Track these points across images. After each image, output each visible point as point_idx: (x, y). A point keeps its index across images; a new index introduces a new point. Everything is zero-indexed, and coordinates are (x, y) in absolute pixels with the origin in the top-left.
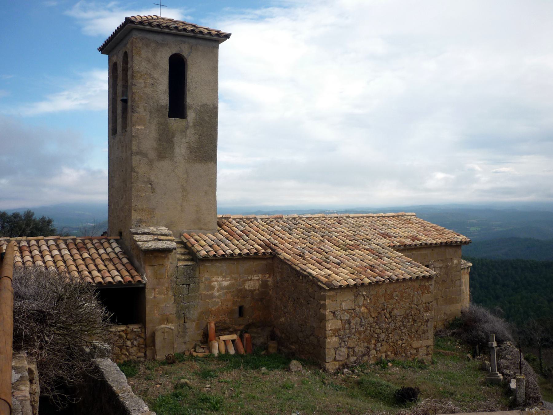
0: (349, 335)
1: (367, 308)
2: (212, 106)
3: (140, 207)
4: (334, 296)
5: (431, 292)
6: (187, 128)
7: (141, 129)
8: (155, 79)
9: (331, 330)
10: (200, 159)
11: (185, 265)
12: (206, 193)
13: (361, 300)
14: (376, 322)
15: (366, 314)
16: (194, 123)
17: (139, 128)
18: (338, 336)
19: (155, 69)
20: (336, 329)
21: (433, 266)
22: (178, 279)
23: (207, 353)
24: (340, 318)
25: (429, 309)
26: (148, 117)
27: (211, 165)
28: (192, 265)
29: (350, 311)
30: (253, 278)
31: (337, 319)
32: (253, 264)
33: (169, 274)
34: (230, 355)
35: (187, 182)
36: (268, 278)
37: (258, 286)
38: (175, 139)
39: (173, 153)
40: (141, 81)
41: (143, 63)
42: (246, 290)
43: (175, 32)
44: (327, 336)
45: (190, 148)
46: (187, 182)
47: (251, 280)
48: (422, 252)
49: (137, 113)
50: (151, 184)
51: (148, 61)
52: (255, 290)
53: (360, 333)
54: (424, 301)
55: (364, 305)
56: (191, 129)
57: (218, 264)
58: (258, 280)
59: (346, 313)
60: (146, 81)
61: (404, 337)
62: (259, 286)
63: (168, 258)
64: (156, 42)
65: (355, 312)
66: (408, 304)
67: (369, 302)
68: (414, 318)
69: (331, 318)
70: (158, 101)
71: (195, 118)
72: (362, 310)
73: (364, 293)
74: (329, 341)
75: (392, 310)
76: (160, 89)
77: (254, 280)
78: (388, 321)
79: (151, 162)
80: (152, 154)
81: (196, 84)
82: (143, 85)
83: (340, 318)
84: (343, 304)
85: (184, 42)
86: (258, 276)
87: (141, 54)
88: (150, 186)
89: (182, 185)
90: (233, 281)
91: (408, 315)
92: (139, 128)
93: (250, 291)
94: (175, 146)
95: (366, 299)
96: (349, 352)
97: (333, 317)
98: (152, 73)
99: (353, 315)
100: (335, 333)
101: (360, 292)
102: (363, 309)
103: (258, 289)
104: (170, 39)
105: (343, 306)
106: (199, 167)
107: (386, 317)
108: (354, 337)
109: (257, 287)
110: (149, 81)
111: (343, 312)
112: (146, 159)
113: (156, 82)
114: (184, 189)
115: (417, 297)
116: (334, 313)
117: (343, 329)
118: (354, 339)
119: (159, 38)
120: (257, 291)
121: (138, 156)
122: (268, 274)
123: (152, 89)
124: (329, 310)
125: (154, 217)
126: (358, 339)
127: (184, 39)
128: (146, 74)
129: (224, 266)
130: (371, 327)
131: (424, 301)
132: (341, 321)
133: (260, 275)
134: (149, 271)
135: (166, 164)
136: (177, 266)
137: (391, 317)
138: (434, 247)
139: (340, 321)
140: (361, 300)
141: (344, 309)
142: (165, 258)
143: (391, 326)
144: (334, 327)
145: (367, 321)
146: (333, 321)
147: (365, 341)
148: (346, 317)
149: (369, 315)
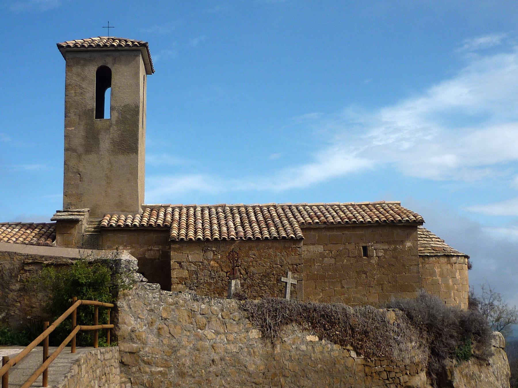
0: (197, 285)
1: (217, 263)
2: (134, 106)
3: (70, 192)
4: (180, 249)
5: (299, 254)
6: (110, 126)
7: (72, 129)
8: (83, 89)
9: (176, 278)
10: (123, 151)
11: (90, 235)
12: (128, 180)
13: (211, 255)
14: (228, 277)
15: (217, 268)
16: (116, 121)
17: (70, 129)
18: (185, 284)
19: (84, 81)
20: (182, 277)
21: (373, 247)
22: (84, 246)
23: (109, 311)
24: (187, 268)
25: (296, 271)
26: (77, 120)
27: (132, 156)
28: (96, 235)
29: (197, 263)
30: (154, 249)
31: (183, 269)
32: (153, 236)
33: (76, 241)
34: (113, 307)
35: (111, 171)
36: (168, 249)
37: (158, 256)
38: (100, 137)
39: (98, 147)
40: (72, 91)
41: (74, 78)
42: (146, 259)
43: (98, 49)
44: (173, 283)
45: (114, 143)
46: (111, 171)
47: (151, 250)
48: (358, 233)
49: (69, 117)
50: (79, 174)
51: (78, 75)
52: (155, 259)
53: (210, 284)
54: (290, 263)
55: (214, 260)
56: (114, 127)
57: (120, 235)
58: (158, 250)
59: (193, 265)
60: (76, 91)
61: (263, 295)
62: (159, 256)
63: (75, 228)
64: (85, 59)
65: (203, 265)
66: (269, 264)
67: (220, 257)
68: (277, 277)
69: (176, 268)
70: (85, 106)
71: (118, 118)
72: (211, 264)
73: (214, 249)
74: (175, 287)
75: (249, 267)
76: (88, 96)
77: (154, 250)
78: (244, 277)
79: (79, 156)
80: (81, 150)
81: (119, 89)
82: (73, 95)
83: (187, 268)
84: (189, 256)
85: (108, 56)
86: (158, 247)
87: (72, 71)
88: (79, 175)
89: (106, 174)
90: (134, 250)
91: (268, 274)
92: (70, 129)
93: (150, 259)
94: (100, 141)
95: (216, 254)
96: (39, 228)
97: (179, 267)
98: (81, 84)
99: (201, 267)
100: (181, 281)
101: (209, 247)
102: (212, 263)
103: (159, 259)
104: (96, 55)
105: (190, 258)
106: (122, 159)
107: (241, 274)
108: (203, 287)
109: (157, 257)
110: (79, 91)
111: (190, 264)
112: (75, 154)
113: (84, 91)
114: (108, 177)
115: (281, 258)
116: (180, 263)
117: (189, 279)
118: (203, 289)
119: (87, 56)
120: (157, 260)
121: (69, 152)
122: (168, 245)
123: (81, 97)
124: (174, 260)
125: (82, 201)
126: (208, 290)
127: (108, 53)
128: (76, 86)
129: (125, 236)
130: (222, 280)
131: (290, 263)
132: (188, 271)
133: (160, 246)
134: (59, 238)
135: (92, 157)
136: (83, 235)
137: (247, 273)
138: (376, 227)
139: (187, 271)
140: (211, 255)
141: (190, 260)
142: (73, 228)
143: (246, 281)
144: (180, 276)
145: (217, 274)
146: (178, 270)
147: (216, 293)
148: (193, 268)
149: (219, 269)
